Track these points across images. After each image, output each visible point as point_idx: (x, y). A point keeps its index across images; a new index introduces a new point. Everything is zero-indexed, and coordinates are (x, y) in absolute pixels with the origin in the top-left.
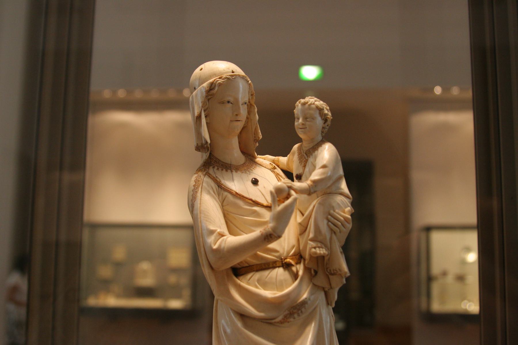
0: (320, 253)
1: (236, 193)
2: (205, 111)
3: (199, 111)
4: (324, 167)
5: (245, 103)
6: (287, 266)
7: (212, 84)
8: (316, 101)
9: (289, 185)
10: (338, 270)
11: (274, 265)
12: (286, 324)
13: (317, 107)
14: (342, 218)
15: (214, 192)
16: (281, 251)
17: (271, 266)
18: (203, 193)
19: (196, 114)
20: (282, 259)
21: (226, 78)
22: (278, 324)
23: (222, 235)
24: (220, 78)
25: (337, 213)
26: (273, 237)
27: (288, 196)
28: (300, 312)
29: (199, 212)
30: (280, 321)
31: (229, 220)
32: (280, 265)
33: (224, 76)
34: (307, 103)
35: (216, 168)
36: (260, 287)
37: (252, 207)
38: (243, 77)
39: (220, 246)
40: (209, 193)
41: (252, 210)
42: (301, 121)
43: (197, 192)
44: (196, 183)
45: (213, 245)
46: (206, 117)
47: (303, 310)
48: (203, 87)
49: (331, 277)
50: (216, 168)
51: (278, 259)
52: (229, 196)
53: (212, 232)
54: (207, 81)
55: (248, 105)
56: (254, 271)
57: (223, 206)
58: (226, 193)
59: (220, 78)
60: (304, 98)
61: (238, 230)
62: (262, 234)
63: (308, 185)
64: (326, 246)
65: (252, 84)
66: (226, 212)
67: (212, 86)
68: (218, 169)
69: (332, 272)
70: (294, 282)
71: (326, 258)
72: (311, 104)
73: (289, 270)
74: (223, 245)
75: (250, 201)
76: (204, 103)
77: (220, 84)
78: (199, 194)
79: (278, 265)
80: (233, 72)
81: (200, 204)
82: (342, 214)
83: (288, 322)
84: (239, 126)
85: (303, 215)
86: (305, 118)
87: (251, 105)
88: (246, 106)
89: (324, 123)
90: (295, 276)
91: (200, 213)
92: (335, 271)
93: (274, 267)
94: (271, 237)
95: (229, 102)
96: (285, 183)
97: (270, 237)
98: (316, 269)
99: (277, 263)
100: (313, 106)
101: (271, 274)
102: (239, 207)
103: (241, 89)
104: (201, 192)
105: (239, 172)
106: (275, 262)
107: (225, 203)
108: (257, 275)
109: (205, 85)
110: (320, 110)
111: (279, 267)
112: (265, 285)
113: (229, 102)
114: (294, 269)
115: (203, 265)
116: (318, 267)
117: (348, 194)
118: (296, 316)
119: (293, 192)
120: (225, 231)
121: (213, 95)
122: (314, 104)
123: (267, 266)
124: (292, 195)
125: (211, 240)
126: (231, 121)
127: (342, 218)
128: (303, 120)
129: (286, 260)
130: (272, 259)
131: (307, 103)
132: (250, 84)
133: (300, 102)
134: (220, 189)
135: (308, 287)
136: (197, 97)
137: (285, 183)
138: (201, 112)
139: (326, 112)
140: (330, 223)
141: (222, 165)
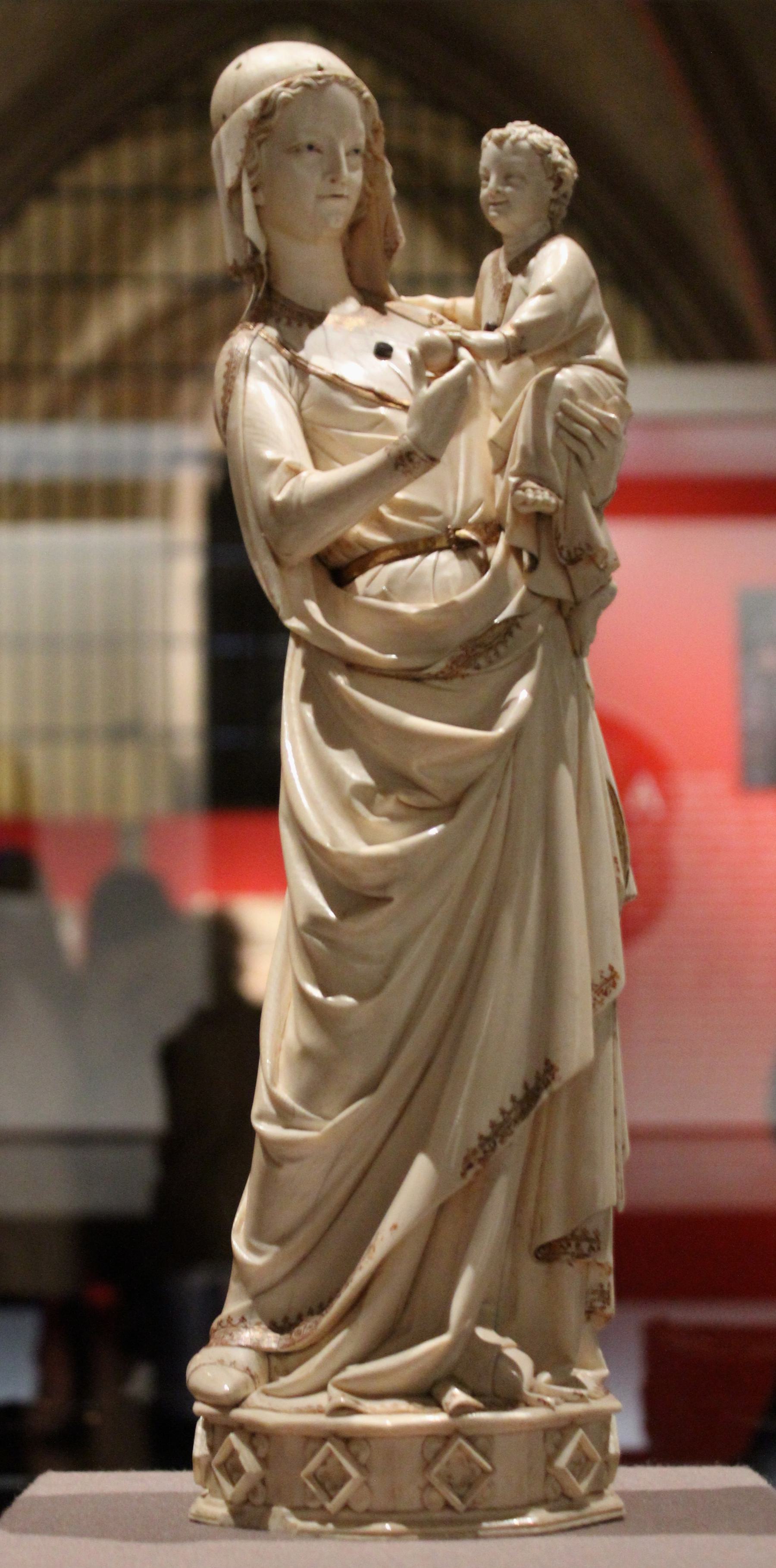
0: (535, 502)
2: (250, 174)
4: (546, 291)
5: (357, 151)
6: (462, 547)
8: (531, 132)
9: (457, 335)
11: (430, 544)
12: (456, 683)
13: (534, 147)
14: (595, 421)
15: (278, 375)
16: (449, 511)
18: (246, 353)
22: (437, 683)
23: (294, 471)
24: (287, 85)
25: (582, 407)
26: (416, 459)
27: (455, 361)
28: (492, 653)
29: (240, 427)
30: (442, 672)
31: (318, 446)
32: (444, 543)
33: (298, 80)
35: (284, 320)
38: (345, 82)
39: (291, 494)
41: (374, 415)
42: (493, 178)
43: (234, 378)
46: (254, 190)
50: (284, 320)
53: (273, 465)
55: (365, 157)
59: (287, 85)
60: (502, 125)
62: (389, 455)
63: (505, 337)
65: (374, 101)
66: (309, 426)
67: (268, 108)
70: (476, 581)
71: (559, 518)
72: (518, 139)
75: (370, 395)
76: (248, 151)
77: (286, 102)
78: (239, 382)
79: (438, 545)
80: (320, 69)
81: (244, 404)
82: (596, 409)
83: (463, 676)
84: (340, 213)
85: (500, 420)
86: (506, 178)
87: (376, 159)
88: (358, 160)
89: (555, 189)
92: (579, 552)
93: (427, 551)
94: (411, 461)
95: (311, 147)
97: (407, 462)
98: (535, 552)
100: (524, 144)
102: (341, 410)
103: (399, 227)
110: (543, 153)
111: (441, 549)
113: (311, 147)
116: (539, 550)
117: (617, 368)
118: (482, 662)
119: (463, 352)
120: (303, 457)
121: (268, 130)
122: (525, 138)
127: (595, 421)
128: (498, 182)
129: (458, 533)
130: (422, 530)
132: (366, 102)
133: (490, 138)
136: (469, 1502)
139: (559, 158)
140: (562, 433)
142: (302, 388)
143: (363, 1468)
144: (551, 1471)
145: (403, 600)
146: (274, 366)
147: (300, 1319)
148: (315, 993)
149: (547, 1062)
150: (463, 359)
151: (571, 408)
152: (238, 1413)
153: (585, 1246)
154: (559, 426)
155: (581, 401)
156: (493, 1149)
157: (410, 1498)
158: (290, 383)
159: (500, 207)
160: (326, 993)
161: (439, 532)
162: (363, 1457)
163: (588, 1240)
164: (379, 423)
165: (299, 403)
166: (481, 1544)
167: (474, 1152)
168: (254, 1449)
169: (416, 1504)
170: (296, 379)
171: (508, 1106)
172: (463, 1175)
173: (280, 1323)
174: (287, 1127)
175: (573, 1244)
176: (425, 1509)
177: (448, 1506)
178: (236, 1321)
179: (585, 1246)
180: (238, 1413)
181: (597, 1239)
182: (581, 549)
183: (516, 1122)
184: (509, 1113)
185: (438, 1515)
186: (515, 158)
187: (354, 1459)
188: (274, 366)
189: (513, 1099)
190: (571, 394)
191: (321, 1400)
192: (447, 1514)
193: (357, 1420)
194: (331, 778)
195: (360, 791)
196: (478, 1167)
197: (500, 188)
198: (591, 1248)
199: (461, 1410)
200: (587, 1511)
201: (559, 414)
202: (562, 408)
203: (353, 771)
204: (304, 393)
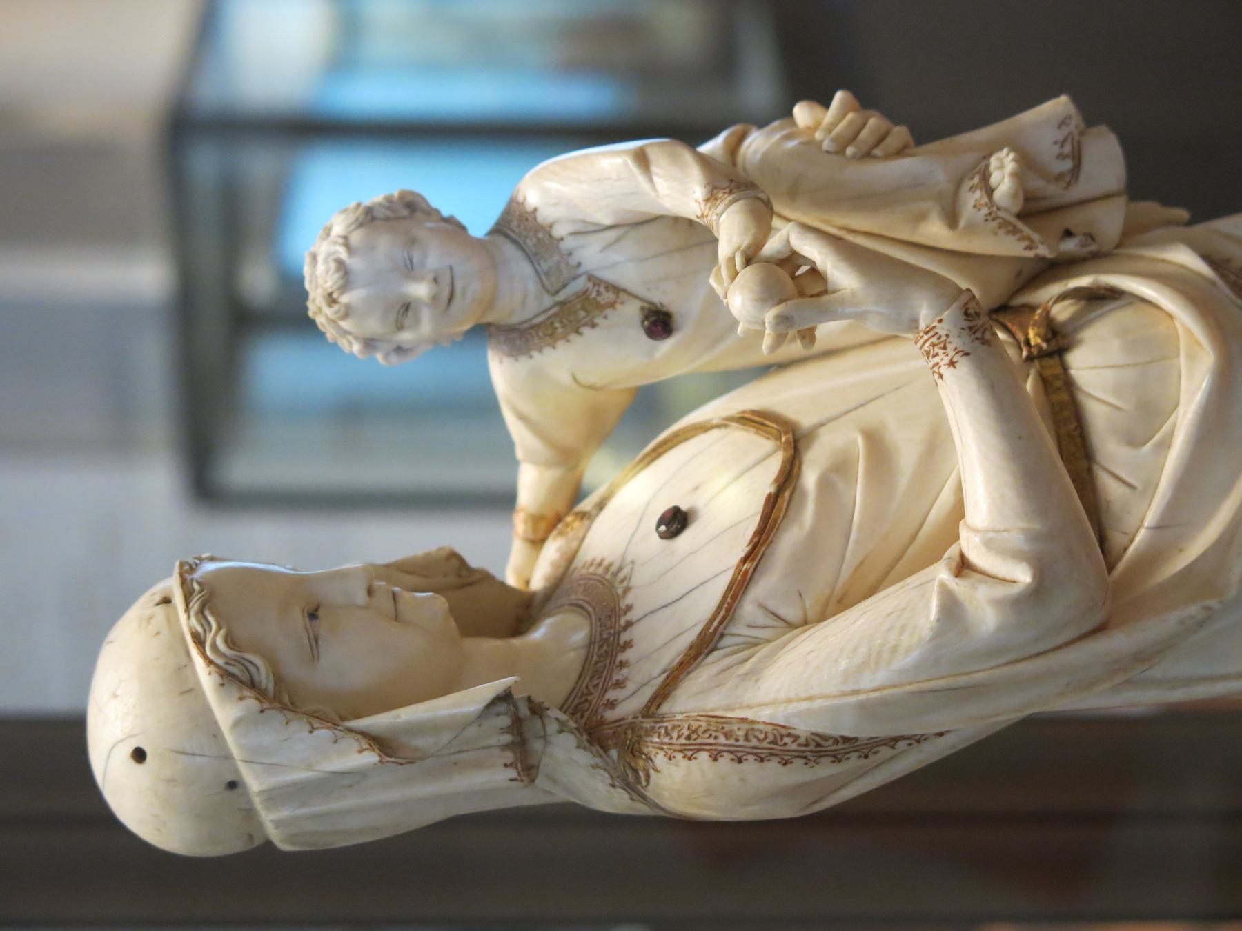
1: (744, 560)
3: (351, 743)
6: (1059, 341)
7: (227, 677)
10: (1065, 130)
11: (1059, 383)
15: (746, 660)
17: (1064, 396)
19: (370, 758)
20: (1030, 359)
21: (201, 611)
27: (790, 260)
29: (853, 699)
34: (340, 264)
36: (1165, 429)
37: (804, 495)
39: (1019, 556)
40: (755, 674)
45: (1014, 590)
48: (237, 724)
51: (1033, 372)
52: (760, 590)
53: (951, 609)
54: (208, 710)
56: (1090, 471)
57: (805, 623)
58: (749, 608)
59: (199, 641)
67: (235, 677)
68: (619, 685)
73: (1077, 330)
74: (1016, 539)
77: (230, 641)
79: (1059, 370)
91: (856, 692)
93: (1069, 385)
99: (1048, 373)
104: (750, 707)
106: (1045, 383)
107: (791, 613)
108: (1111, 451)
109: (226, 711)
111: (1065, 368)
112: (1148, 416)
114: (1062, 312)
119: (772, 246)
123: (1066, 413)
125: (985, 611)
126: (396, 618)
131: (340, 264)
134: (727, 641)
135: (1142, 258)
138: (364, 734)
141: (597, 674)
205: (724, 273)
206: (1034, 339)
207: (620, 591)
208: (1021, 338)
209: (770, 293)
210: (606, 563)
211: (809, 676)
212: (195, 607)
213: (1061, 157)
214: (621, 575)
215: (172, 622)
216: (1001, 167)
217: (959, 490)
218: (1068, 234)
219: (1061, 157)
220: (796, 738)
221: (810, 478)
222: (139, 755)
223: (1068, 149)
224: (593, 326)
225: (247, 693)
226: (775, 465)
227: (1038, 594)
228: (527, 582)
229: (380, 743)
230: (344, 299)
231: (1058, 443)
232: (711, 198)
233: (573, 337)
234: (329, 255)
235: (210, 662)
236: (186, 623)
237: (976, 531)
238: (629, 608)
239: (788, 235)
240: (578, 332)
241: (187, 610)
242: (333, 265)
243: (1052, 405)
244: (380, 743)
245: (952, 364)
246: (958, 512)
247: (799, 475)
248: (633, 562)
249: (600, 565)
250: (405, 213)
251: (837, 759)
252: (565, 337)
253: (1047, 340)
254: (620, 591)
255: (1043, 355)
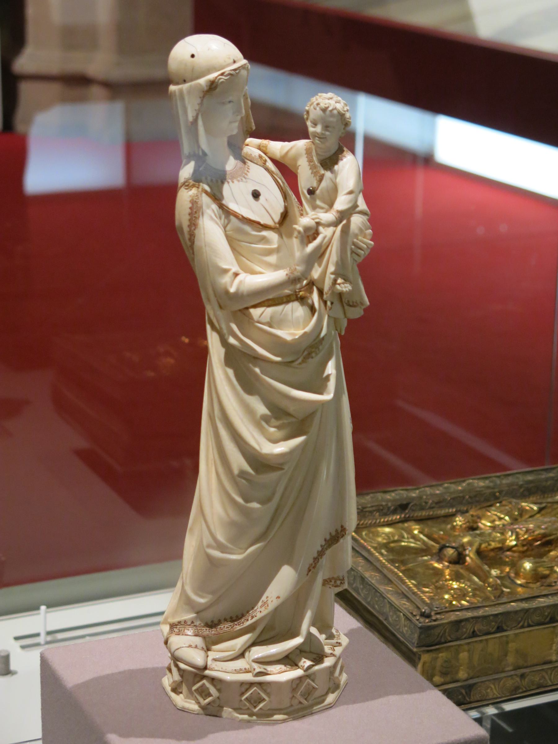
1: (242, 216)
6: (302, 300)
11: (288, 299)
14: (365, 246)
19: (191, 119)
20: (296, 292)
27: (316, 234)
32: (294, 297)
37: (260, 231)
39: (238, 289)
41: (259, 236)
44: (193, 204)
47: (321, 347)
49: (346, 307)
53: (226, 271)
59: (222, 74)
61: (244, 259)
62: (289, 278)
64: (351, 283)
67: (213, 86)
69: (351, 304)
79: (292, 299)
90: (312, 309)
91: (205, 246)
93: (288, 302)
96: (313, 219)
101: (285, 309)
102: (247, 234)
105: (331, 284)
106: (289, 296)
109: (203, 81)
111: (293, 301)
113: (230, 102)
115: (209, 300)
118: (313, 355)
124: (321, 233)
125: (226, 280)
127: (365, 246)
137: (313, 219)
142: (226, 221)
143: (268, 694)
144: (332, 677)
145: (280, 328)
146: (213, 211)
147: (220, 622)
148: (240, 500)
149: (342, 527)
150: (321, 233)
151: (358, 243)
152: (207, 672)
153: (338, 582)
154: (352, 252)
155: (360, 238)
156: (318, 562)
157: (286, 703)
158: (220, 218)
159: (321, 140)
160: (247, 501)
161: (292, 293)
162: (268, 691)
163: (340, 580)
164: (264, 240)
165: (225, 228)
166: (315, 717)
167: (312, 564)
168: (215, 686)
169: (289, 705)
170: (223, 217)
171: (323, 543)
172: (307, 574)
173: (210, 623)
174: (222, 552)
175: (333, 581)
176: (292, 706)
177: (300, 703)
178: (189, 623)
179: (338, 582)
180: (207, 672)
181: (343, 579)
182: (356, 303)
183: (327, 549)
184: (324, 546)
185: (296, 707)
186: (331, 119)
187: (265, 691)
188: (213, 211)
189: (325, 540)
190: (356, 236)
191: (240, 664)
192: (300, 706)
193: (268, 678)
194: (249, 411)
195: (265, 418)
196: (312, 570)
197: (323, 132)
198: (341, 583)
199: (310, 667)
200: (341, 685)
201: (353, 247)
202: (354, 244)
203: (262, 409)
204: (227, 225)
205: (314, 217)
206: (301, 293)
207: (239, 179)
208: (302, 290)
209: (307, 229)
210: (248, 173)
211: (212, 233)
212: (232, 72)
213: (353, 302)
214: (244, 179)
215: (228, 65)
216: (345, 287)
217: (261, 273)
218: (332, 303)
219: (353, 302)
220: (195, 229)
221: (265, 233)
222: (193, 56)
223: (355, 304)
224: (312, 173)
225: (208, 88)
226: (270, 223)
227: (227, 292)
228: (247, 145)
229: (195, 121)
230: (318, 109)
231: (271, 297)
232: (338, 212)
233: (309, 167)
234: (330, 104)
235: (216, 77)
236: (228, 70)
237: (245, 278)
238: (233, 182)
239: (325, 232)
240: (311, 169)
241: (231, 70)
242: (327, 106)
243: (283, 297)
244: (195, 121)
245: (287, 275)
246: (253, 272)
247: (266, 230)
248: (247, 182)
249: (248, 171)
250: (344, 123)
251: (190, 239)
252: (309, 165)
253: (301, 296)
254: (239, 179)
255: (296, 295)
